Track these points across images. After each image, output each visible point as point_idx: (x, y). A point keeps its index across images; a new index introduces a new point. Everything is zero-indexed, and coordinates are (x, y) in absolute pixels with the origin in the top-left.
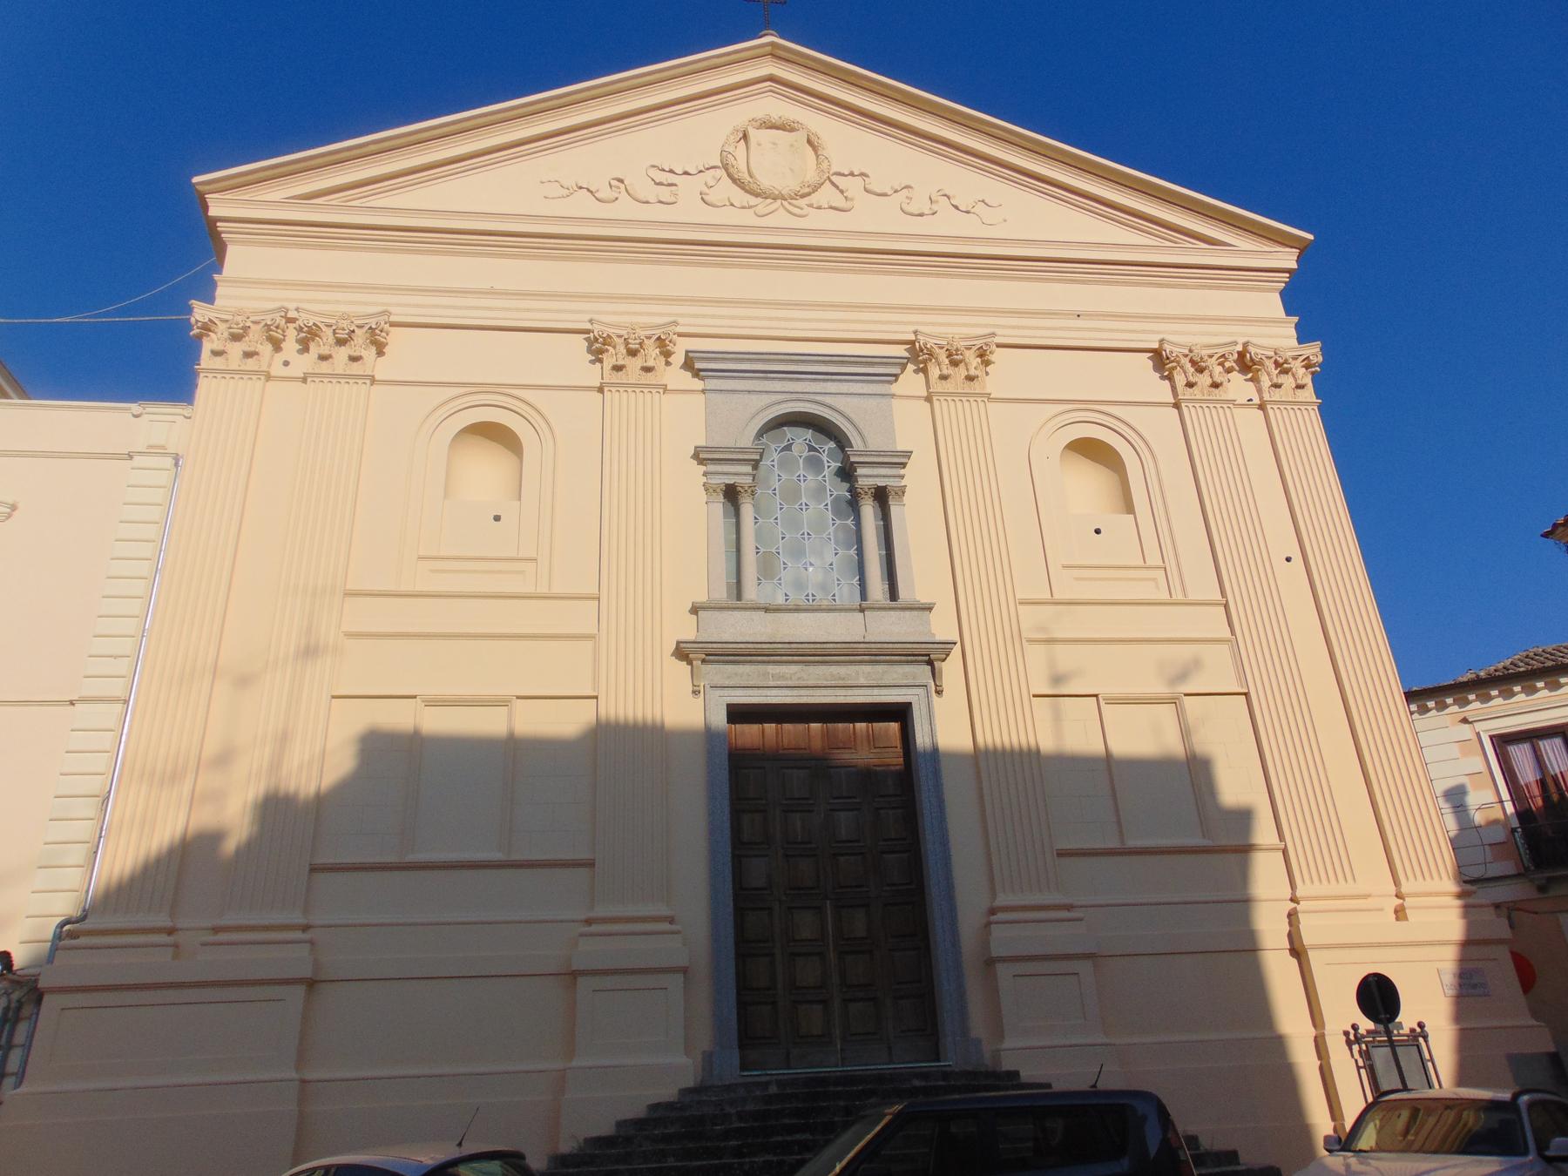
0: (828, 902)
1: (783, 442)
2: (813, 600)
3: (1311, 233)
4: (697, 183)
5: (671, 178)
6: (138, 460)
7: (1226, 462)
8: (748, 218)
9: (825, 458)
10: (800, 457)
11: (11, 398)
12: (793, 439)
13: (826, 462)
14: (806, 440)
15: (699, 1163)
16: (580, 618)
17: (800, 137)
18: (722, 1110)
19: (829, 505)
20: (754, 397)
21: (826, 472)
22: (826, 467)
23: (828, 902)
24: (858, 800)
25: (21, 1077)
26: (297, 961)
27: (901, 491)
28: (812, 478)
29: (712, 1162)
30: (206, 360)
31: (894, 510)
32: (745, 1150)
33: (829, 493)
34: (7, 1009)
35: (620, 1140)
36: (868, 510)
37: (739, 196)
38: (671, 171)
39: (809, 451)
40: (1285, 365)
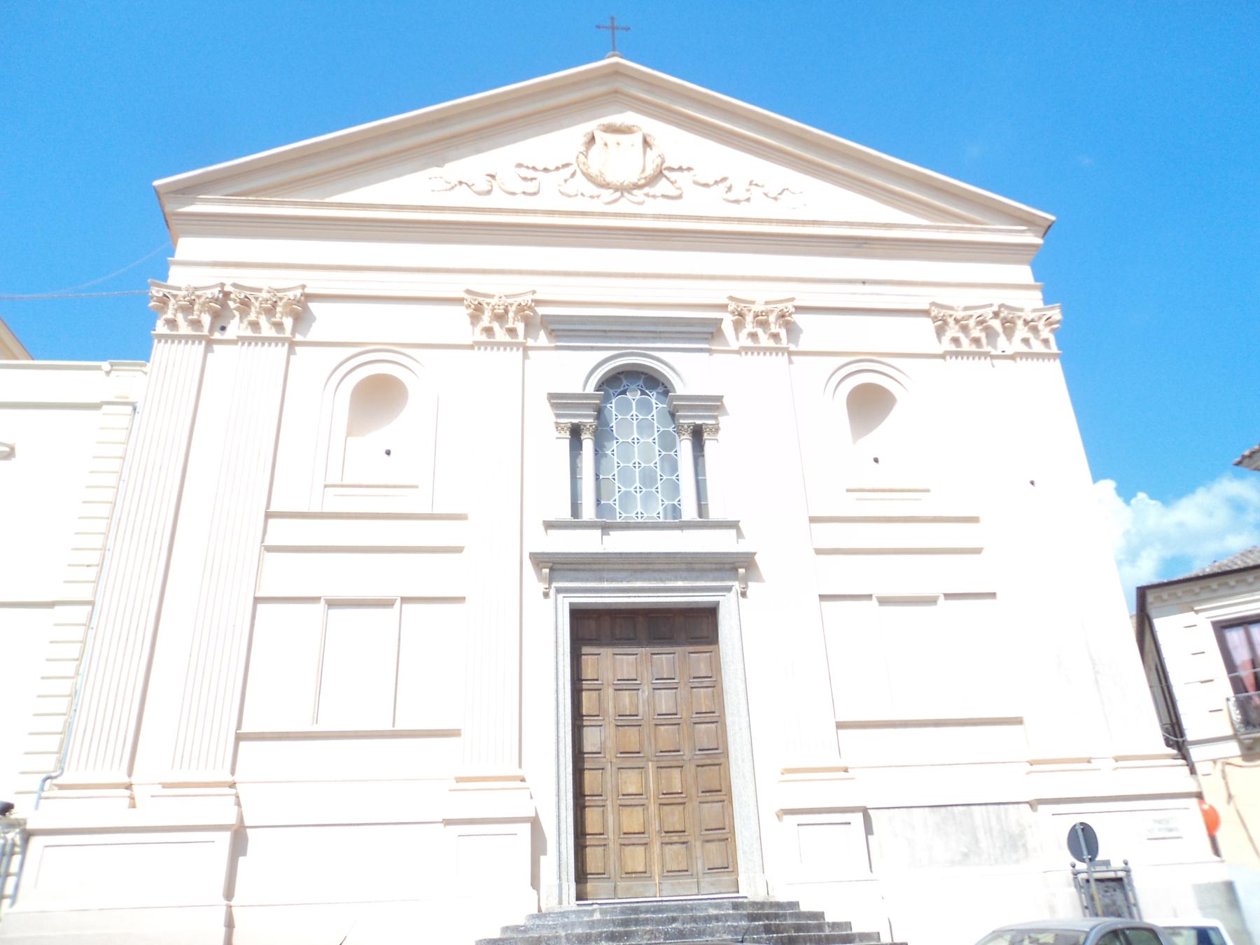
0: (650, 764)
2: (642, 517)
5: (530, 174)
10: (634, 400)
11: (16, 358)
12: (628, 385)
14: (638, 386)
16: (281, 532)
17: (637, 139)
18: (557, 932)
21: (654, 412)
22: (654, 408)
23: (650, 764)
25: (14, 898)
27: (716, 429)
30: (161, 328)
31: (709, 446)
34: (4, 845)
38: (534, 168)
39: (641, 395)
40: (1032, 323)
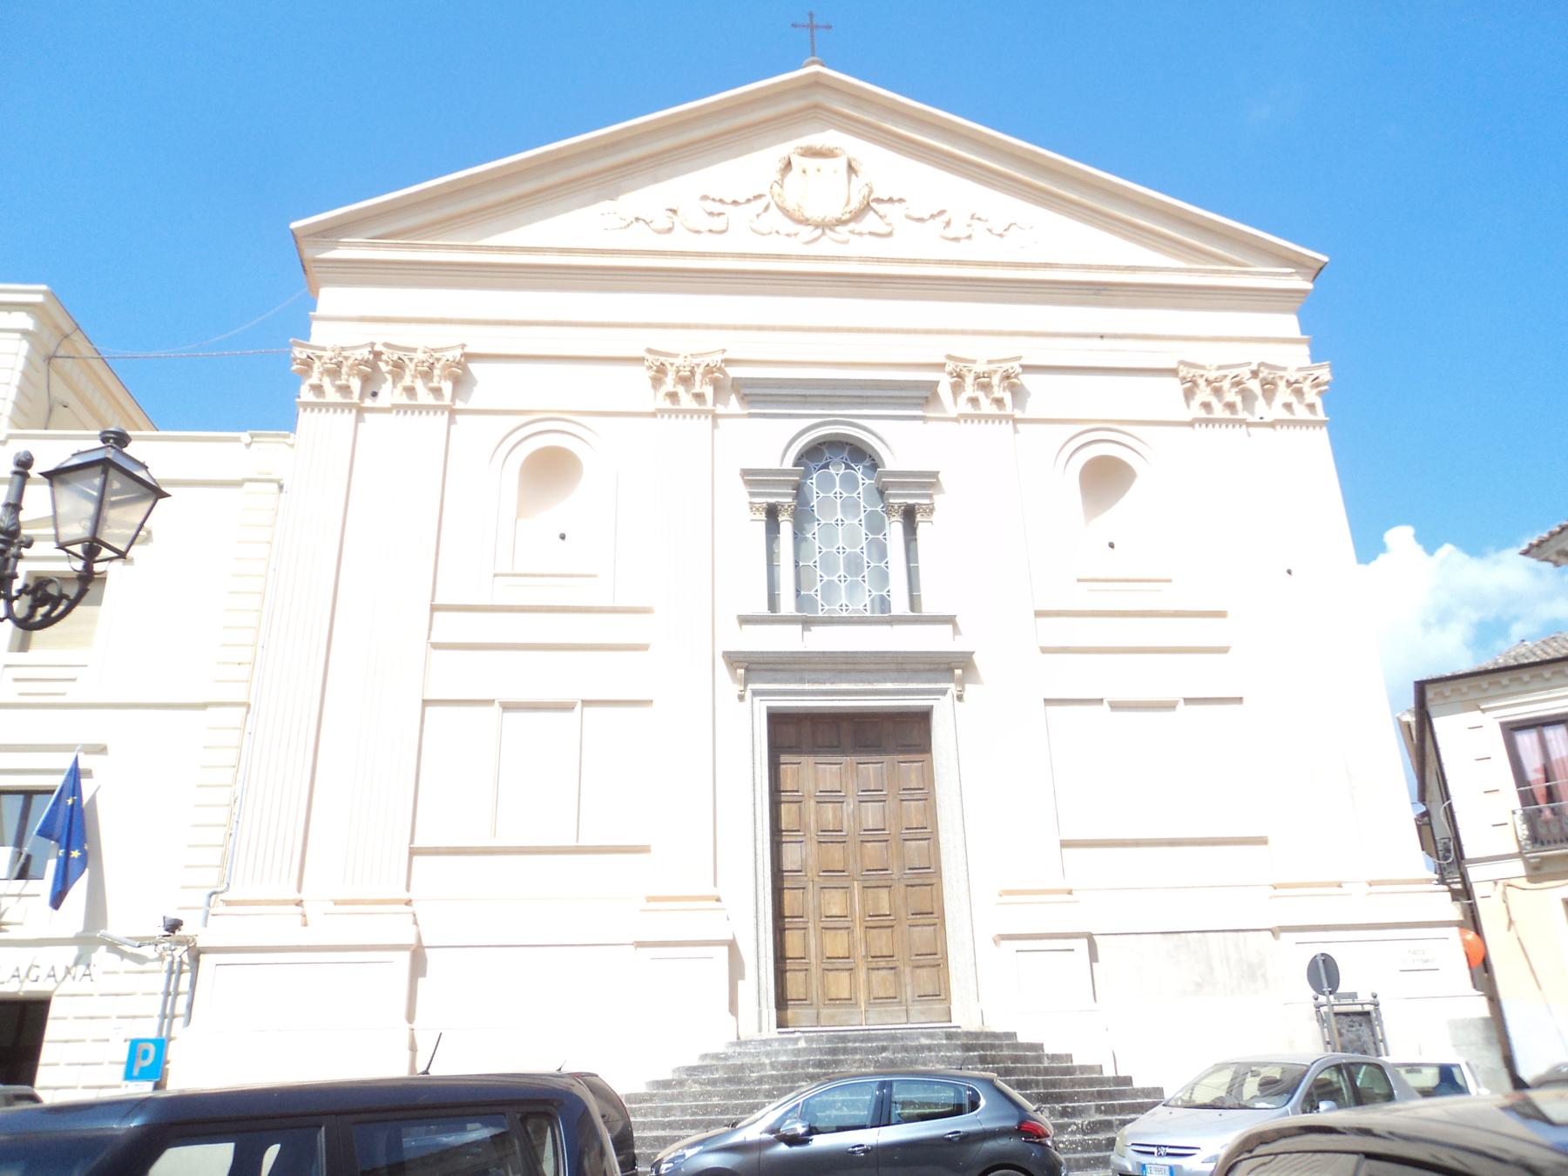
0: (856, 883)
1: (821, 461)
5: (717, 208)
9: (860, 476)
10: (837, 474)
14: (842, 458)
15: (737, 1102)
17: (840, 164)
19: (865, 548)
21: (861, 489)
22: (861, 485)
24: (883, 793)
29: (748, 1101)
30: (306, 395)
31: (923, 529)
32: (775, 1093)
33: (868, 593)
35: (674, 1083)
36: (895, 529)
37: (788, 226)
38: (721, 201)
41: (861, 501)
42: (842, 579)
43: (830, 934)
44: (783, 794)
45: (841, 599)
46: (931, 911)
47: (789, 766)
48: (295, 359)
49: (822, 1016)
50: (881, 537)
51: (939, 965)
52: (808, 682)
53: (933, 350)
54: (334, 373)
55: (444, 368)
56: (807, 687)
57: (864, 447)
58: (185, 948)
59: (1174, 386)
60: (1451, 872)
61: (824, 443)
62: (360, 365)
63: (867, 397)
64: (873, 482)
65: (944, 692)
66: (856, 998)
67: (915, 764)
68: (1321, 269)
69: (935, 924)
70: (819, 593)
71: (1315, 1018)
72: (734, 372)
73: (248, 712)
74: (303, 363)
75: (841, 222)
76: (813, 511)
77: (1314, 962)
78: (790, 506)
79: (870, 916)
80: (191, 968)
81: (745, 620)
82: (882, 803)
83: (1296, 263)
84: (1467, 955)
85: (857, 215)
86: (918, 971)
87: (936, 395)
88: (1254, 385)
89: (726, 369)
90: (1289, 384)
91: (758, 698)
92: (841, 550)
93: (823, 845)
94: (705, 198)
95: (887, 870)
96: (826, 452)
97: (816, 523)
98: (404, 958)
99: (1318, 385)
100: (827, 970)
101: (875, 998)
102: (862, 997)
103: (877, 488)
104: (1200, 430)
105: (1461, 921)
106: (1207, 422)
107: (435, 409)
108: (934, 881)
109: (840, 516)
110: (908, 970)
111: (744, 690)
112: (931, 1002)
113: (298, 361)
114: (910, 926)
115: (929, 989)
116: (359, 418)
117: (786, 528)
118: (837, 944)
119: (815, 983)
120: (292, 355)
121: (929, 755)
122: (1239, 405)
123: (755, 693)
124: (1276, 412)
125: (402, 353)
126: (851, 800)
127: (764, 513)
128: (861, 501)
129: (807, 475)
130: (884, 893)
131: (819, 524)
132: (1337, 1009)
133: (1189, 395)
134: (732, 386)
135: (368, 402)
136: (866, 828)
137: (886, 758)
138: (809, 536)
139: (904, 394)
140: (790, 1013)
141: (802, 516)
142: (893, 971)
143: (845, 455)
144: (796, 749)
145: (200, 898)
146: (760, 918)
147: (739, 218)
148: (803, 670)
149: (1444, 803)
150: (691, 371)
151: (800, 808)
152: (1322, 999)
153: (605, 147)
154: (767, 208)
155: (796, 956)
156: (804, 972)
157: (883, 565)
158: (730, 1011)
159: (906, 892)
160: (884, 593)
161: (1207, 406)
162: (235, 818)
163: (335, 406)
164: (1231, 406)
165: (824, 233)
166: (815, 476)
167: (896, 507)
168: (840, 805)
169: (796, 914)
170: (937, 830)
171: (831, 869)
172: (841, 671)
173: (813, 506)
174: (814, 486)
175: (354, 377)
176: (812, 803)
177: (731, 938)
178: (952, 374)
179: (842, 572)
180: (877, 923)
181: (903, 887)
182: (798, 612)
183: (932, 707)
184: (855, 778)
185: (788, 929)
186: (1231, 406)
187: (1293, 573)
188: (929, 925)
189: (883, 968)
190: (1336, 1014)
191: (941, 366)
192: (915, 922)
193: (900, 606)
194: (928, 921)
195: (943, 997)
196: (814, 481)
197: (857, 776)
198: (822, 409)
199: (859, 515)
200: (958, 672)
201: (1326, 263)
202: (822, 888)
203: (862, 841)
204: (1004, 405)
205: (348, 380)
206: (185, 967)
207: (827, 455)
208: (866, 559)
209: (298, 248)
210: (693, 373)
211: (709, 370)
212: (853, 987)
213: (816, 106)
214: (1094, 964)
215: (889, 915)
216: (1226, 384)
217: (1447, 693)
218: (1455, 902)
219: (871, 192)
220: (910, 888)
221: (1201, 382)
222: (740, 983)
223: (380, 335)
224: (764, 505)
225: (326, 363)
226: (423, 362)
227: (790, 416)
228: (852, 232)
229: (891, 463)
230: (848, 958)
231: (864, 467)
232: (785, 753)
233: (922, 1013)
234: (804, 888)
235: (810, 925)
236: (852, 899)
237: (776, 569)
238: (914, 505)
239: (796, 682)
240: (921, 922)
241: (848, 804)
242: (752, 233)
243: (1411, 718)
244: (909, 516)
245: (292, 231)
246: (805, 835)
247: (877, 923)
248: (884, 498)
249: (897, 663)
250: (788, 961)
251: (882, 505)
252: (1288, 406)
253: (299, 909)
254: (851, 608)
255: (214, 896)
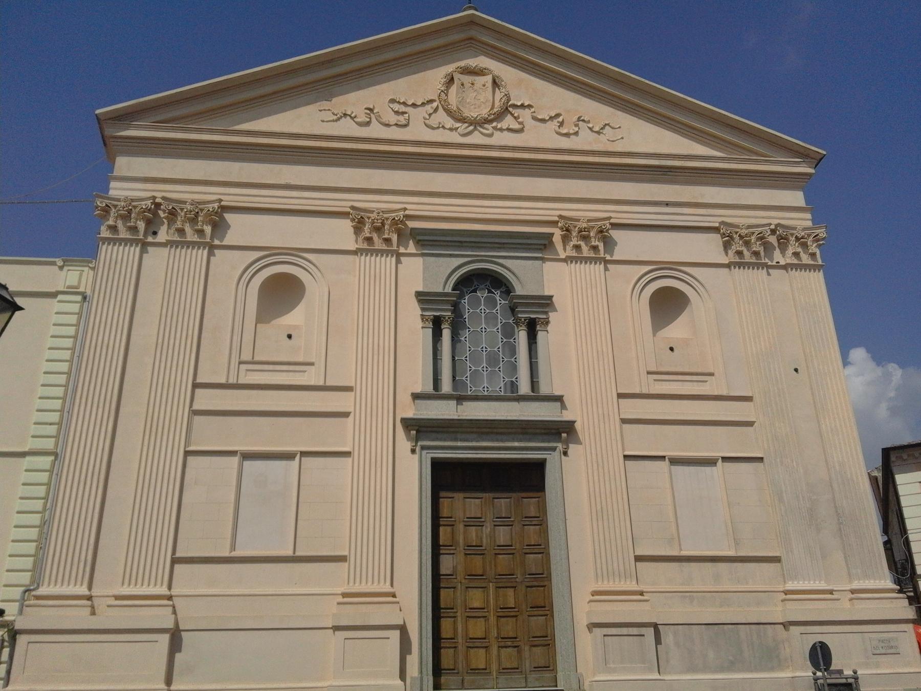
0: (491, 584)
3: (824, 150)
4: (422, 112)
5: (402, 108)
6: (60, 297)
7: (365, 356)
8: (455, 138)
9: (498, 298)
10: (482, 297)
13: (498, 300)
14: (486, 286)
20: (453, 259)
21: (498, 307)
22: (498, 304)
26: (162, 618)
28: (489, 311)
30: (105, 233)
31: (541, 335)
36: (522, 336)
37: (449, 122)
41: (499, 315)
42: (485, 369)
43: (472, 621)
44: (441, 519)
45: (484, 383)
46: (543, 605)
47: (446, 499)
48: (97, 207)
49: (465, 681)
50: (512, 340)
51: (549, 645)
52: (460, 441)
53: (551, 211)
54: (126, 217)
55: (206, 215)
56: (459, 444)
57: (504, 280)
58: (6, 630)
59: (716, 238)
60: (907, 584)
61: (474, 275)
62: (145, 212)
63: (504, 243)
64: (507, 302)
65: (554, 449)
66: (490, 668)
67: (534, 499)
68: (821, 159)
69: (547, 615)
70: (468, 379)
71: (814, 687)
72: (412, 224)
73: (56, 459)
74: (103, 209)
75: (488, 121)
76: (465, 321)
77: (814, 648)
78: (449, 318)
79: (501, 608)
80: (10, 644)
81: (416, 397)
82: (510, 527)
83: (804, 155)
84: (919, 643)
85: (499, 116)
86: (534, 649)
87: (551, 243)
88: (773, 239)
89: (406, 222)
90: (797, 239)
91: (426, 451)
92: (484, 349)
93: (468, 556)
94: (393, 101)
95: (513, 575)
96: (475, 280)
97: (467, 330)
98: (165, 639)
99: (818, 240)
100: (470, 647)
101: (503, 669)
102: (494, 667)
103: (510, 307)
104: (736, 271)
105: (915, 619)
106: (740, 265)
107: (131, 242)
108: (546, 583)
109: (484, 326)
110: (527, 648)
111: (416, 446)
112: (543, 672)
113: (99, 208)
114: (529, 616)
115: (542, 663)
116: (143, 251)
117: (446, 334)
118: (477, 629)
119: (461, 658)
120: (95, 204)
121: (543, 493)
122: (762, 254)
123: (423, 448)
124: (789, 259)
125: (174, 204)
126: (488, 525)
127: (431, 323)
128: (499, 315)
129: (461, 296)
130: (510, 592)
131: (469, 331)
132: (829, 681)
133: (727, 246)
134: (411, 234)
135: (150, 239)
136: (499, 544)
137: (514, 495)
138: (463, 339)
139: (529, 241)
140: (443, 679)
141: (457, 326)
142: (516, 649)
143: (488, 283)
144: (453, 487)
145: (17, 593)
146: (423, 610)
147: (416, 116)
148: (457, 432)
149: (902, 537)
150: (382, 223)
151: (453, 529)
152: (819, 674)
153: (323, 63)
154: (436, 110)
155: (448, 637)
156: (454, 649)
157: (513, 360)
158: (400, 677)
159: (526, 592)
160: (514, 380)
161: (739, 253)
162: (45, 536)
163: (125, 241)
164: (756, 254)
165: (475, 129)
166: (467, 297)
167: (523, 320)
168: (480, 528)
169: (449, 606)
170: (549, 546)
171: (473, 573)
172: (482, 433)
173: (465, 318)
174: (466, 305)
175: (140, 221)
176: (461, 526)
177: (402, 623)
178: (563, 228)
179: (485, 365)
180: (505, 613)
181: (524, 588)
182: (453, 391)
183: (546, 459)
184: (492, 508)
185: (443, 617)
186: (756, 254)
187: (799, 371)
188: (542, 616)
189: (509, 646)
190: (829, 685)
191: (554, 223)
192: (533, 613)
193: (524, 388)
194: (541, 613)
195: (551, 668)
196: (466, 301)
197: (493, 507)
198: (472, 251)
199: (496, 325)
200: (564, 435)
201: (825, 155)
202: (467, 588)
203: (496, 554)
204: (599, 251)
205: (136, 223)
206: (6, 644)
207: (476, 283)
208: (501, 355)
209: (100, 128)
210: (383, 224)
211: (395, 222)
212: (489, 662)
213: (471, 39)
214: (658, 646)
215: (514, 608)
216: (753, 238)
217: (905, 457)
218: (911, 606)
219: (509, 100)
220: (529, 589)
221: (736, 237)
222: (408, 657)
223: (161, 191)
224: (432, 316)
225: (120, 211)
226: (191, 212)
227: (451, 256)
228: (495, 128)
229: (519, 290)
230: (485, 639)
231: (501, 292)
232: (443, 490)
233: (537, 679)
234: (454, 588)
235: (459, 614)
236: (488, 596)
237: (439, 361)
238: (535, 319)
239: (451, 440)
240: (536, 613)
241: (486, 527)
242: (424, 125)
243: (878, 474)
244: (532, 328)
245: (96, 115)
246: (456, 549)
247: (505, 613)
248: (515, 313)
249: (522, 428)
250: (442, 641)
251: (513, 318)
252: (796, 254)
253: (89, 603)
254: (490, 389)
255: (27, 594)
